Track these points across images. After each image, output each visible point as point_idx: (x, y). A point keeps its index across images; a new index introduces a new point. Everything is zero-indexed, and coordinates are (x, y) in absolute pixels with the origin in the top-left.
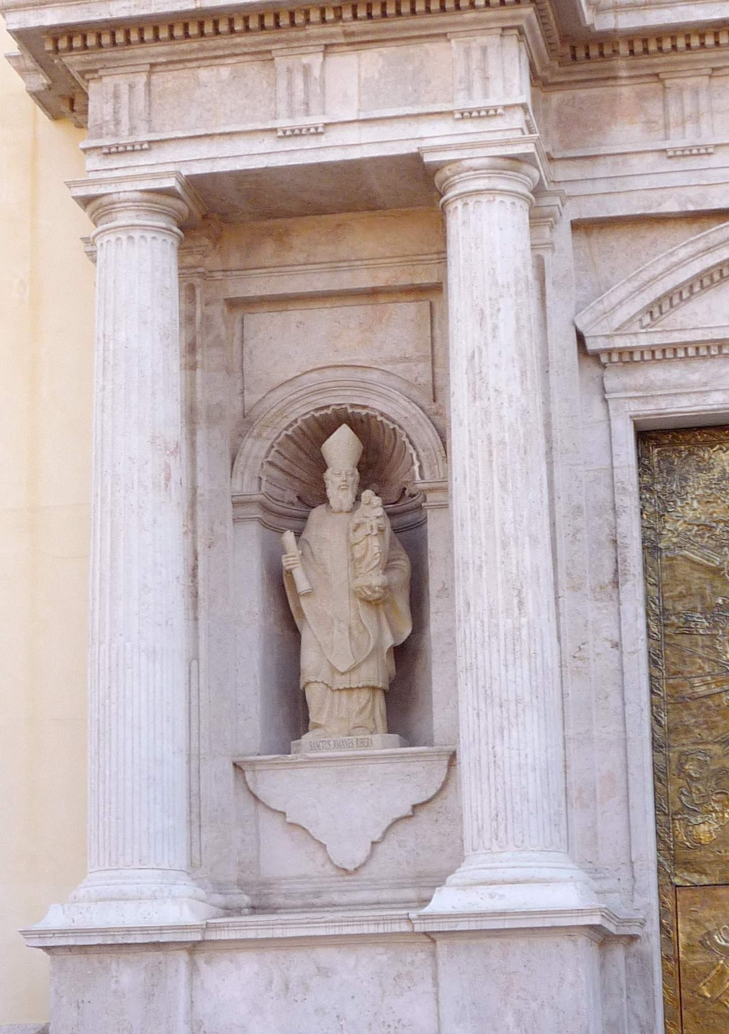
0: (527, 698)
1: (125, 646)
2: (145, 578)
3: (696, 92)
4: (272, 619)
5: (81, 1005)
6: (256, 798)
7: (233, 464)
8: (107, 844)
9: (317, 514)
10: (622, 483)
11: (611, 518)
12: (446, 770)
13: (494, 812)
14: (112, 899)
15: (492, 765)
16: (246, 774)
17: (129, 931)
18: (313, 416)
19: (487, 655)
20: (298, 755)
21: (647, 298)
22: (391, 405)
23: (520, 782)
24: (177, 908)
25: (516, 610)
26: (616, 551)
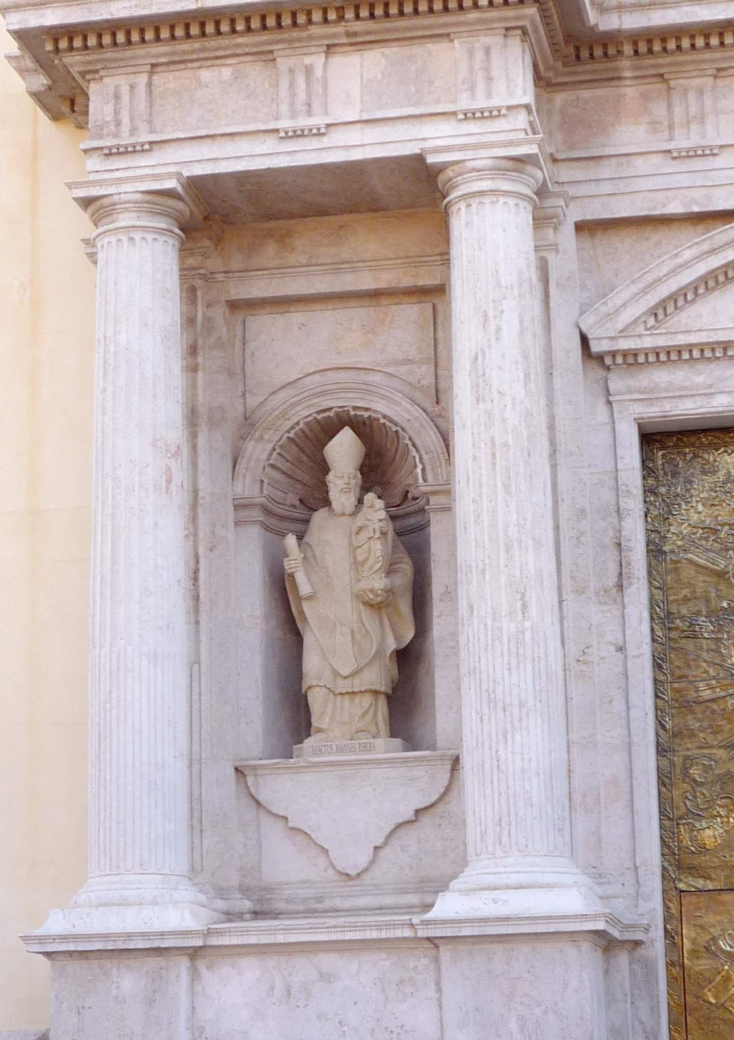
0: (531, 702)
1: (126, 650)
2: (146, 581)
3: (701, 93)
4: (273, 623)
5: (81, 1011)
6: (257, 802)
7: (234, 467)
8: (108, 849)
9: (319, 517)
10: (627, 485)
11: (615, 521)
12: (449, 775)
13: (497, 817)
14: (113, 905)
15: (495, 769)
16: (248, 778)
17: (129, 936)
18: (315, 418)
19: (490, 658)
20: (300, 760)
21: (652, 299)
22: (393, 408)
23: (524, 786)
25: (520, 613)
26: (621, 554)
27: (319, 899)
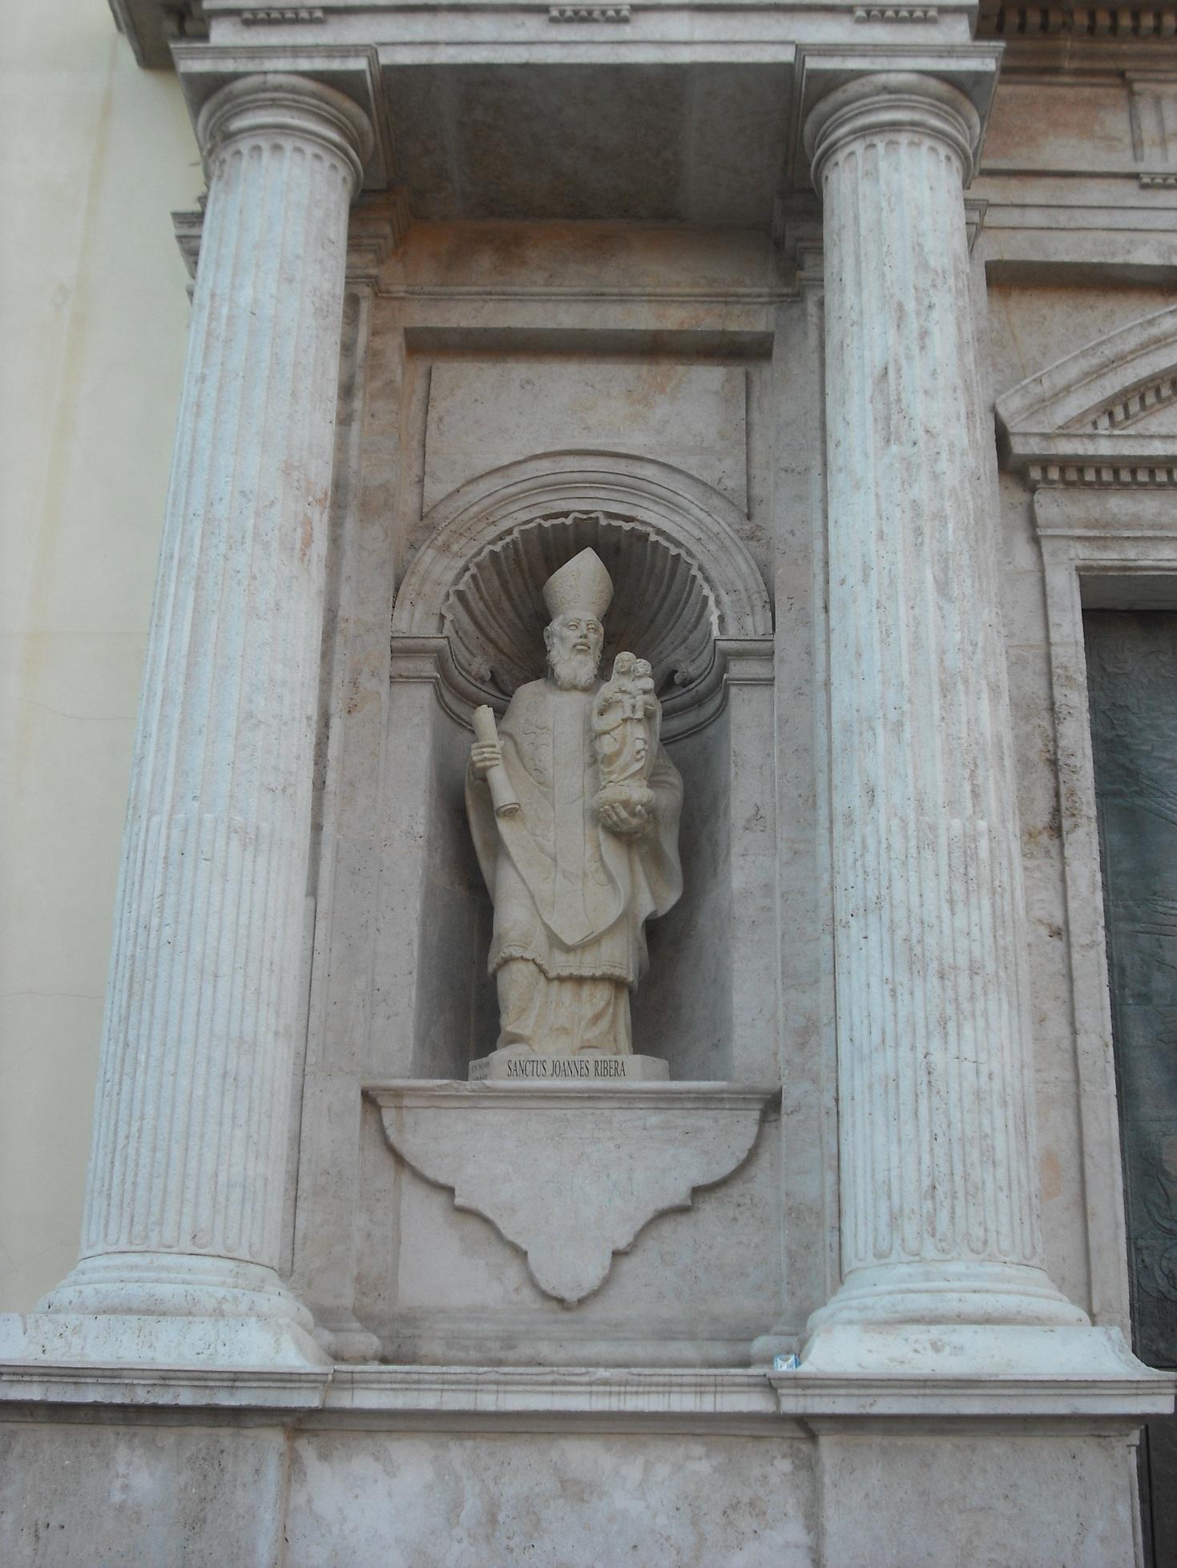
0: (990, 968)
1: (200, 821)
2: (251, 701)
4: (437, 860)
5: (42, 1533)
6: (399, 1159)
7: (397, 590)
8: (127, 1200)
9: (528, 693)
10: (1066, 668)
11: (1046, 724)
12: (755, 1129)
13: (927, 1182)
14: (130, 1311)
15: (924, 1088)
16: (384, 1112)
17: (166, 1377)
18: (540, 525)
19: (913, 880)
21: (1113, 384)
22: (678, 520)
23: (980, 1125)
24: (267, 1342)
25: (969, 804)
26: (1056, 777)
27: (509, 1342)
